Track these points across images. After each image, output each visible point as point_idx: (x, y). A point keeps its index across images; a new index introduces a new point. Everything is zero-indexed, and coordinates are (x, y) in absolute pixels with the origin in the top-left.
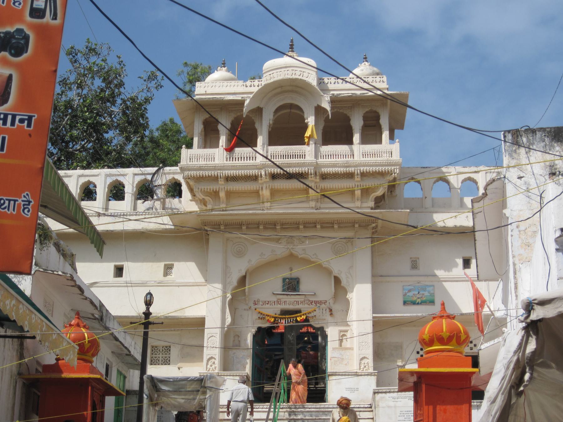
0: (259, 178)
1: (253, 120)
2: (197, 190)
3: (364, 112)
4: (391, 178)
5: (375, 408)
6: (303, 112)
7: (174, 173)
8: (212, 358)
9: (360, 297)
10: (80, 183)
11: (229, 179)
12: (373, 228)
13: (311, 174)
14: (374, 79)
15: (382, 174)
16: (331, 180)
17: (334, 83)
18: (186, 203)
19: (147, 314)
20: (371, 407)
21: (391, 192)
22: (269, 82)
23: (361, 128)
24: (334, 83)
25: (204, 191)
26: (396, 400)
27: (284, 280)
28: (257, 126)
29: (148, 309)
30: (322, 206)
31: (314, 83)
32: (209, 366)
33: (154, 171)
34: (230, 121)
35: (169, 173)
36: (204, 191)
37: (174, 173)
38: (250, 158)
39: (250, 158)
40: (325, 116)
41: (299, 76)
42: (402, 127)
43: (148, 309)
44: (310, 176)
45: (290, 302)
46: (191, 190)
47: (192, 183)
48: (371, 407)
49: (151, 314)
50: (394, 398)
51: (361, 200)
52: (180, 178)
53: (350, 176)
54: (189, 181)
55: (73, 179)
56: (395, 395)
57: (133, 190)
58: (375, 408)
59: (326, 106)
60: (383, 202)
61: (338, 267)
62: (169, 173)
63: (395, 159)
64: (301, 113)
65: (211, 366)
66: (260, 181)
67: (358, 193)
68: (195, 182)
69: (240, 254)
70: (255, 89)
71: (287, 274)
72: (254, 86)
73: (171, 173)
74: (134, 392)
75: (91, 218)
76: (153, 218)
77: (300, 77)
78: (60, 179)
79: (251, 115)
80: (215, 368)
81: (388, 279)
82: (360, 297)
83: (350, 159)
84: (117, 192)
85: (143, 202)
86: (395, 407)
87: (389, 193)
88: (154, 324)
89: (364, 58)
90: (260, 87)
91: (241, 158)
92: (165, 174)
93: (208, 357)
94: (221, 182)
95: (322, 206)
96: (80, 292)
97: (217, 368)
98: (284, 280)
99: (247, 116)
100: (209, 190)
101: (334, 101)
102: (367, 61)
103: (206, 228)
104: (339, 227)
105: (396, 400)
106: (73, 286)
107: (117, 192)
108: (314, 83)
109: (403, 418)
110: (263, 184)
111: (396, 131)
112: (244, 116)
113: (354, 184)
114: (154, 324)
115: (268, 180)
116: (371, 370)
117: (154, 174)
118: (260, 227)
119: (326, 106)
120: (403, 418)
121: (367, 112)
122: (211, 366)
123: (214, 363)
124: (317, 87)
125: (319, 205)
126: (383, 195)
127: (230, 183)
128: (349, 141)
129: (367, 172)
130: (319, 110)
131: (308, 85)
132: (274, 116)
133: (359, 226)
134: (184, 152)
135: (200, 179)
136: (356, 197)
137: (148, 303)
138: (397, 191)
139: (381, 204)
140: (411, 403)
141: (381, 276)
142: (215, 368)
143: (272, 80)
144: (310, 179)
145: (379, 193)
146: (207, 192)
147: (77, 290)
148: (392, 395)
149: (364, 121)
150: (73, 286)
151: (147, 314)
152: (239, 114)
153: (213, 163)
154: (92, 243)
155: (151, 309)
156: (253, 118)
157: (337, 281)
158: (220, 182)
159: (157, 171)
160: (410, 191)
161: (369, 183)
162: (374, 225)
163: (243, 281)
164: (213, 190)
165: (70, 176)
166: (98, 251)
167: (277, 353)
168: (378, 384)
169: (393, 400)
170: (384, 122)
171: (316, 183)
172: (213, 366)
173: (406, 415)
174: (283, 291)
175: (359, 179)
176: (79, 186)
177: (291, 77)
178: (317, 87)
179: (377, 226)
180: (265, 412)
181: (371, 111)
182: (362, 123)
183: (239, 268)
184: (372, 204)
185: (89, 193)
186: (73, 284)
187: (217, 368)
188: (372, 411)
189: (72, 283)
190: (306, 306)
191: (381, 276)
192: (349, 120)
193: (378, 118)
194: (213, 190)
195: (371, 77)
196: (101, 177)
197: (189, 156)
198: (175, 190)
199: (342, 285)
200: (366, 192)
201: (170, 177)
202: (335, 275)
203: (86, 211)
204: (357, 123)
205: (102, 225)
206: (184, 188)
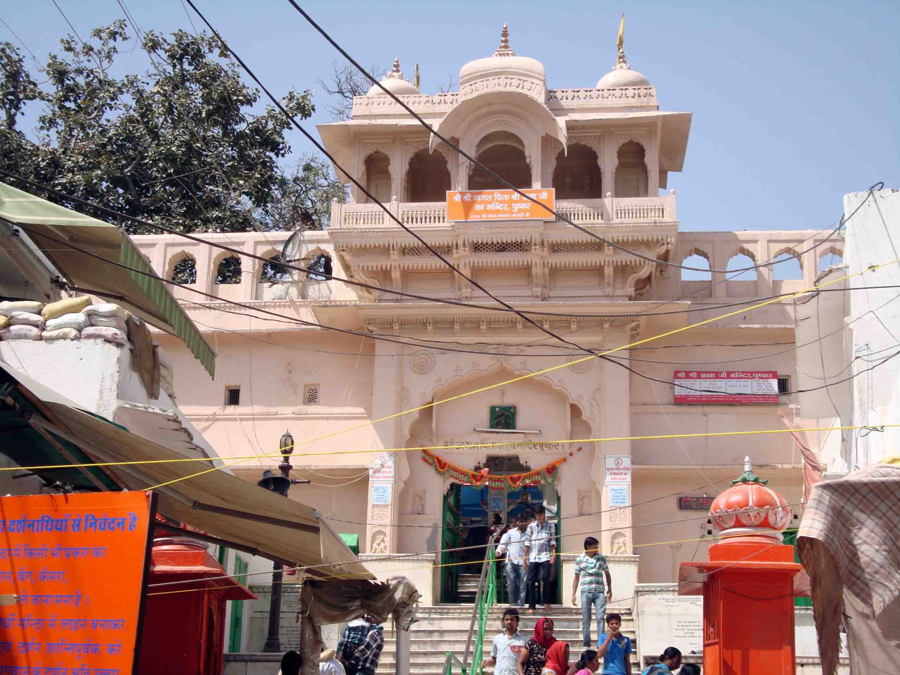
0: (454, 251)
1: (444, 157)
2: (356, 268)
3: (620, 144)
4: (662, 250)
5: (638, 615)
6: (523, 146)
7: (319, 241)
8: (380, 532)
9: (613, 436)
10: (169, 256)
11: (406, 251)
12: (633, 329)
13: (535, 244)
14: (636, 92)
15: (648, 244)
16: (566, 253)
17: (367, 105)
18: (339, 291)
19: (286, 468)
20: (630, 614)
21: (662, 271)
22: (469, 97)
23: (614, 171)
24: (367, 105)
25: (368, 269)
26: (671, 604)
27: (493, 409)
28: (450, 167)
29: (286, 459)
30: (552, 294)
31: (541, 99)
32: (375, 545)
33: (287, 238)
34: (409, 160)
35: (311, 241)
36: (368, 269)
37: (319, 241)
38: (439, 218)
39: (439, 218)
40: (558, 151)
41: (518, 87)
42: (679, 169)
43: (286, 459)
44: (533, 247)
45: (502, 444)
46: (347, 268)
47: (347, 257)
48: (630, 614)
49: (290, 467)
50: (667, 600)
51: (614, 285)
52: (329, 249)
53: (598, 246)
54: (343, 253)
55: (158, 248)
56: (670, 596)
57: (254, 268)
58: (638, 615)
59: (562, 137)
60: (648, 287)
61: (578, 390)
62: (311, 241)
63: (669, 220)
64: (520, 148)
65: (379, 544)
66: (455, 255)
67: (609, 271)
68: (354, 256)
69: (422, 370)
70: (448, 109)
71: (497, 401)
72: (445, 103)
73: (312, 242)
74: (261, 589)
75: (191, 314)
76: (281, 307)
77: (519, 90)
78: (134, 248)
79: (440, 150)
80: (385, 548)
81: (650, 409)
82: (613, 436)
83: (596, 221)
84: (228, 270)
85: (271, 286)
86: (669, 615)
87: (658, 274)
88: (295, 483)
89: (620, 57)
90: (455, 105)
91: (426, 218)
92: (304, 242)
93: (374, 531)
94: (395, 255)
95: (552, 294)
96: (188, 439)
97: (388, 548)
98: (493, 409)
99: (435, 151)
100: (375, 268)
101: (572, 127)
102: (624, 62)
103: (371, 328)
104: (579, 327)
105: (671, 604)
106: (176, 430)
107: (228, 270)
108: (541, 99)
109: (682, 633)
110: (459, 259)
111: (670, 174)
112: (431, 152)
113: (607, 257)
114: (295, 483)
115: (468, 253)
116: (629, 553)
117: (287, 243)
118: (455, 327)
119: (562, 137)
120: (682, 633)
121: (624, 145)
122: (379, 544)
123: (383, 540)
124: (545, 106)
125: (547, 292)
126: (649, 278)
127: (407, 257)
128: (528, 183)
129: (623, 241)
130: (548, 141)
131: (529, 102)
132: (477, 151)
133: (611, 326)
134: (335, 206)
135: (362, 251)
136: (606, 280)
137: (287, 452)
138: (671, 271)
139: (645, 290)
140: (700, 610)
141: (645, 404)
142: (385, 548)
143: (475, 95)
144: (533, 251)
145: (644, 273)
146: (372, 271)
147: (184, 436)
148: (665, 596)
149: (619, 157)
150: (176, 430)
151: (286, 468)
152: (422, 148)
153: (381, 226)
154: (188, 347)
155: (292, 462)
156: (444, 154)
157: (575, 411)
158: (392, 257)
159: (291, 238)
160: (694, 270)
161: (624, 258)
162: (634, 324)
163: (427, 413)
164: (382, 269)
165: (152, 245)
166: (207, 369)
167: (473, 519)
168: (642, 577)
169: (667, 604)
170: (652, 160)
171: (542, 258)
172: (382, 545)
173: (686, 628)
174: (491, 427)
175: (611, 252)
176: (167, 261)
177: (504, 90)
178: (545, 106)
179: (638, 326)
180: (467, 619)
181: (631, 143)
182: (616, 162)
183: (421, 390)
184: (631, 291)
185: (184, 268)
186: (175, 426)
187: (388, 548)
188: (632, 620)
189: (175, 426)
190: (527, 449)
191: (645, 404)
192: (597, 157)
193: (640, 152)
194: (382, 269)
195: (630, 88)
196: (205, 248)
197: (343, 214)
198: (321, 267)
199: (583, 418)
200: (622, 271)
201: (312, 247)
202: (573, 402)
203: (180, 302)
204: (608, 163)
205: (205, 322)
206: (336, 265)
